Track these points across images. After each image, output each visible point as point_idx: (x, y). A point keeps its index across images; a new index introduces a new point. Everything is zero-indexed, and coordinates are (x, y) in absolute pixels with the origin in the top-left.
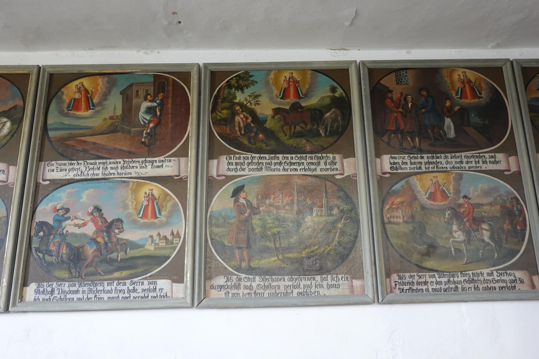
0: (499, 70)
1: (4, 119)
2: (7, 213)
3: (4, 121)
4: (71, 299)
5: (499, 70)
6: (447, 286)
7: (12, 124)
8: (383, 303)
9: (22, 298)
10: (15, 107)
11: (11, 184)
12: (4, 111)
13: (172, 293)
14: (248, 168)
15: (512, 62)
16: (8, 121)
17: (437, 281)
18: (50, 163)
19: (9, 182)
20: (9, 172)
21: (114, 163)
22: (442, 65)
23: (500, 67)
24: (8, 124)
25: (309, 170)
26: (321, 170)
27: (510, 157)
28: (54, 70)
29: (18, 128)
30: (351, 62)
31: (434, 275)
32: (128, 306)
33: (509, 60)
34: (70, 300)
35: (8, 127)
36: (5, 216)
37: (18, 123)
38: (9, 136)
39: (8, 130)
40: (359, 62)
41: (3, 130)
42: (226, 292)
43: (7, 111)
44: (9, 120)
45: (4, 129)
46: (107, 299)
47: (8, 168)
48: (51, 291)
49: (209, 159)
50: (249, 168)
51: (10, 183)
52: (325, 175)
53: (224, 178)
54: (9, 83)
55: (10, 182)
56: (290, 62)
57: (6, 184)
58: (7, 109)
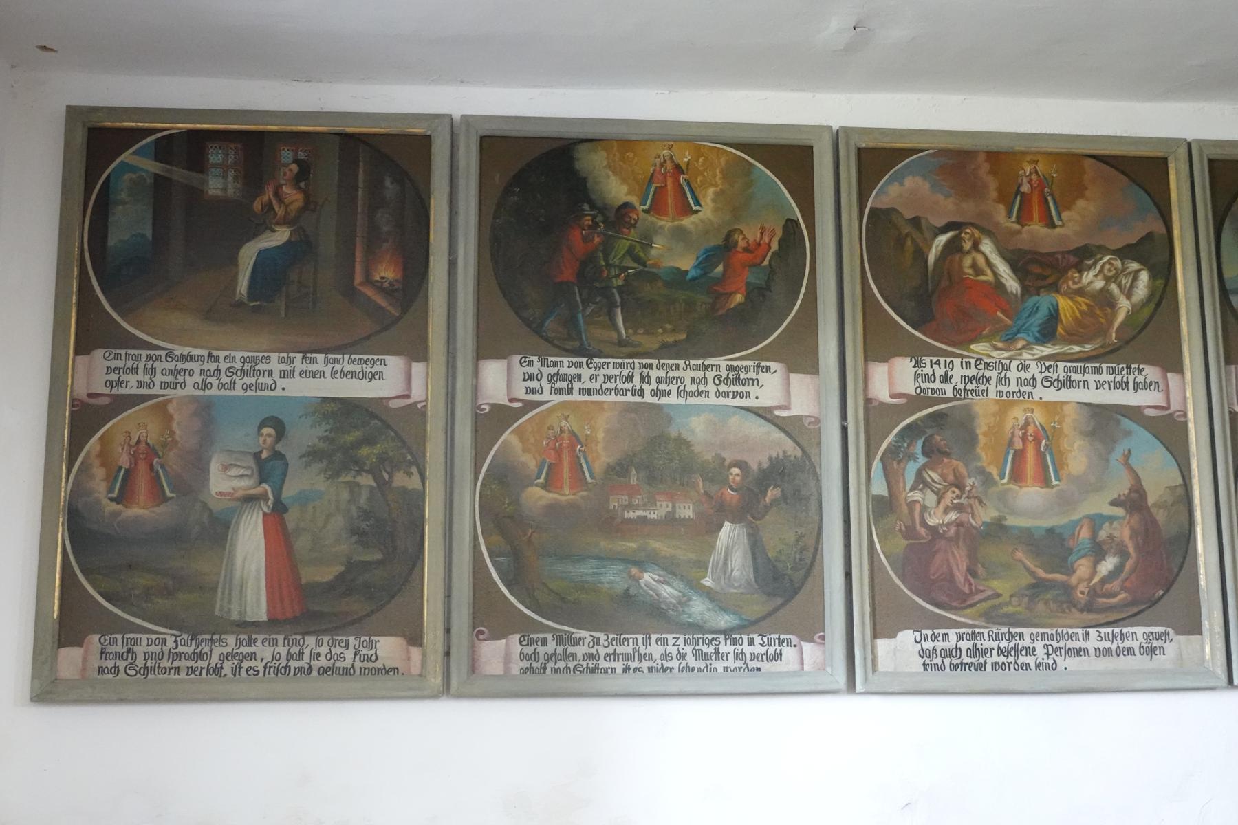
0: (805, 153)
1: (1133, 265)
2: (1183, 477)
3: (1134, 269)
4: (609, 671)
5: (805, 153)
6: (982, 660)
7: (1153, 277)
8: (460, 696)
9: (473, 668)
10: (1149, 236)
11: (1178, 413)
12: (1128, 246)
13: (802, 664)
14: (634, 383)
15: (1189, 144)
16: (1143, 269)
17: (922, 648)
18: (527, 359)
19: (1173, 408)
20: (1167, 386)
21: (697, 367)
22: (1019, 147)
23: (809, 146)
24: (1144, 276)
25: (601, 392)
26: (582, 391)
27: (416, 364)
28: (1219, 151)
29: (1166, 285)
30: (1176, 142)
31: (546, 639)
32: (675, 686)
33: (1186, 140)
34: (606, 672)
35: (1146, 283)
36: (1180, 485)
37: (1164, 272)
38: (1152, 306)
39: (1146, 290)
40: (837, 128)
41: (1135, 289)
42: (234, 666)
43: (1135, 244)
44: (1142, 267)
45: (1137, 288)
46: (722, 671)
47: (1166, 378)
48: (299, 653)
49: (478, 359)
50: (632, 385)
51: (1175, 412)
52: (229, 396)
53: (519, 405)
54: (1122, 177)
55: (1175, 409)
56: (592, 119)
57: (1167, 412)
58: (1134, 242)
